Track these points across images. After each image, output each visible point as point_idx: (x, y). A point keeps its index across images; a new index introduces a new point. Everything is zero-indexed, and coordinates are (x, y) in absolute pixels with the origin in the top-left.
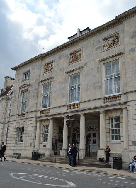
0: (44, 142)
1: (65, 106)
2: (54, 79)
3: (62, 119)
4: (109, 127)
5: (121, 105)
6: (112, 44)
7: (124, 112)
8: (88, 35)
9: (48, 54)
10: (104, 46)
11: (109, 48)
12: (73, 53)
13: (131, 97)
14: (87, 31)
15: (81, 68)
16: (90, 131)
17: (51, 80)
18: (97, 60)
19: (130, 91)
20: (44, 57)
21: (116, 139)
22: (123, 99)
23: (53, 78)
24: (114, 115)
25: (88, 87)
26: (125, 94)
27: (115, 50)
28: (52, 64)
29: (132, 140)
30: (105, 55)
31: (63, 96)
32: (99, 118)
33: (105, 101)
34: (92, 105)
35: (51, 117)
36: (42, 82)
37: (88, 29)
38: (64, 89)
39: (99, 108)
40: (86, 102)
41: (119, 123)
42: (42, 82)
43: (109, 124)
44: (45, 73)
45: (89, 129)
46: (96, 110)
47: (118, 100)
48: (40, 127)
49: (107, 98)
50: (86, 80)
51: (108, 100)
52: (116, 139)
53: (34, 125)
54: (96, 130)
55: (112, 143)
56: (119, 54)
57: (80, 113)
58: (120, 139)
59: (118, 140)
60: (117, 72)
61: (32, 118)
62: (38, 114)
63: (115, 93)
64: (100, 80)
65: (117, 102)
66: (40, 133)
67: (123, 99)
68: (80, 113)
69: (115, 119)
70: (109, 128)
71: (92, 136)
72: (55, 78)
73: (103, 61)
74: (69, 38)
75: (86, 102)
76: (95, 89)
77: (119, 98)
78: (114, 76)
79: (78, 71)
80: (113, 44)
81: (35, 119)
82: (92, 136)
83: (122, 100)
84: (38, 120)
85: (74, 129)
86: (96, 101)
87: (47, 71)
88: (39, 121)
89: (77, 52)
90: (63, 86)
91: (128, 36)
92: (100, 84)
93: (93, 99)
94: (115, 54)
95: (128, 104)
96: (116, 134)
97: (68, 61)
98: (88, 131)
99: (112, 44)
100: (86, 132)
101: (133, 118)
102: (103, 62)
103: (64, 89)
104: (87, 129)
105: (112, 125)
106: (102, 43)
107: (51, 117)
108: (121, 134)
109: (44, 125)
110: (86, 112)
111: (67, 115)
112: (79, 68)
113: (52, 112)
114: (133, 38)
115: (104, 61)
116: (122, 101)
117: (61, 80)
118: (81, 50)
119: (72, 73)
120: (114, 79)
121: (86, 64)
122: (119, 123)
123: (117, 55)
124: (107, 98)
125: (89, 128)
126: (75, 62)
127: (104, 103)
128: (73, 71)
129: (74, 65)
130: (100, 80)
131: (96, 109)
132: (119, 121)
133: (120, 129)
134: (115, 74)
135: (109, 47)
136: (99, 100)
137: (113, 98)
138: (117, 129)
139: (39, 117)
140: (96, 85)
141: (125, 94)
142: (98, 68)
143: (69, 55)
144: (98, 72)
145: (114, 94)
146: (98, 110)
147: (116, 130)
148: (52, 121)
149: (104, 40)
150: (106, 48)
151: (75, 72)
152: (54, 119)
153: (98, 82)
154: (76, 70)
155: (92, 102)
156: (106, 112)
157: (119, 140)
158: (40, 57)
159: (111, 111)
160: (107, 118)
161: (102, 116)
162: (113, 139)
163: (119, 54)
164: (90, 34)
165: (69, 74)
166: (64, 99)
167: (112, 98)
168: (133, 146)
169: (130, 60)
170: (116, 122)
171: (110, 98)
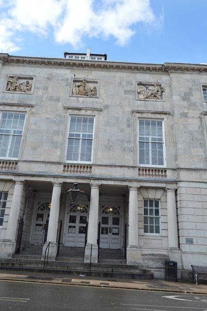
1: (60, 163)
2: (33, 110)
7: (170, 195)
8: (114, 66)
9: (24, 61)
10: (139, 93)
11: (146, 99)
12: (81, 81)
14: (103, 59)
15: (98, 111)
16: (42, 209)
17: (27, 109)
18: (128, 109)
19: (182, 167)
20: (12, 61)
21: (150, 232)
22: (170, 175)
23: (32, 106)
24: (152, 195)
25: (111, 144)
26: (173, 169)
27: (158, 105)
28: (30, 81)
29: (185, 235)
30: (140, 105)
31: (55, 145)
35: (23, 179)
37: (105, 56)
38: (57, 133)
39: (131, 181)
40: (106, 166)
41: (5, 201)
44: (8, 92)
45: (116, 211)
47: (12, 168)
51: (153, 172)
52: (152, 231)
54: (119, 214)
55: (147, 238)
57: (92, 182)
59: (154, 234)
60: (159, 136)
64: (132, 139)
67: (170, 175)
68: (92, 182)
69: (151, 201)
71: (78, 220)
72: (35, 108)
73: (138, 112)
74: (66, 54)
75: (106, 166)
76: (124, 150)
78: (12, 132)
79: (89, 113)
80: (154, 96)
85: (104, 208)
86: (126, 169)
87: (15, 90)
89: (88, 82)
90: (56, 128)
91: (178, 95)
92: (132, 145)
93: (119, 165)
94: (153, 110)
95: (180, 184)
96: (151, 223)
98: (70, 211)
100: (100, 215)
103: (57, 133)
104: (102, 211)
106: (134, 87)
107: (23, 179)
110: (104, 182)
111: (62, 180)
112: (94, 109)
113: (22, 168)
115: (139, 114)
117: (52, 116)
119: (76, 112)
121: (107, 107)
122: (5, 201)
124: (144, 169)
125: (42, 205)
128: (80, 109)
129: (81, 99)
130: (132, 139)
131: (125, 182)
132: (6, 198)
133: (4, 210)
134: (17, 130)
135: (147, 98)
136: (131, 169)
137: (11, 164)
141: (173, 169)
142: (128, 121)
144: (129, 126)
146: (129, 184)
148: (136, 192)
150: (141, 97)
151: (83, 112)
152: (27, 185)
153: (130, 142)
154: (86, 109)
155: (118, 169)
156: (140, 189)
157: (157, 234)
158: (4, 57)
159: (147, 188)
160: (141, 198)
161: (133, 196)
162: (146, 231)
163: (165, 114)
164: (131, 67)
165: (70, 111)
166: (58, 152)
168: (188, 245)
169: (181, 127)
170: (151, 207)
171: (10, 163)
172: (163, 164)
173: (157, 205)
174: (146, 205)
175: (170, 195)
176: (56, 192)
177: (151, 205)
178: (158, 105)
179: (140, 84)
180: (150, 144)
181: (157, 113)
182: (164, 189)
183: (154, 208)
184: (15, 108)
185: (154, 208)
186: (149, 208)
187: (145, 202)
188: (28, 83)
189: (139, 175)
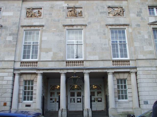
0: (25, 101)
1: (63, 61)
2: (44, 28)
3: (58, 76)
4: (128, 86)
5: (61, 70)
6: (118, 14)
7: (133, 76)
12: (72, 8)
13: (140, 63)
17: (40, 28)
18: (104, 23)
21: (122, 99)
23: (43, 26)
24: (122, 76)
27: (35, 22)
30: (111, 20)
32: (59, 78)
33: (22, 64)
34: (101, 65)
35: (42, 72)
36: (23, 26)
39: (61, 69)
42: (23, 26)
43: (23, 86)
46: (105, 71)
47: (25, 65)
48: (20, 82)
49: (32, 62)
50: (90, 39)
52: (123, 99)
53: (11, 78)
56: (126, 25)
57: (84, 71)
58: (126, 98)
59: (124, 100)
61: (6, 70)
62: (18, 66)
63: (32, 58)
65: (126, 66)
66: (19, 90)
67: (132, 64)
68: (84, 71)
70: (23, 90)
71: (76, 95)
77: (36, 64)
79: (79, 27)
80: (119, 14)
81: (12, 70)
82: (76, 95)
83: (131, 64)
84: (16, 72)
87: (31, 16)
88: (19, 74)
96: (122, 94)
97: (65, 14)
99: (118, 14)
101: (143, 82)
102: (110, 27)
105: (118, 86)
106: (106, 10)
108: (34, 96)
109: (24, 80)
114: (138, 16)
116: (131, 66)
118: (41, 9)
119: (71, 28)
120: (32, 46)
121: (89, 23)
123: (81, 25)
124: (70, 61)
126: (76, 17)
127: (21, 66)
128: (73, 26)
132: (32, 84)
138: (29, 91)
139: (19, 70)
140: (104, 46)
143: (65, 8)
145: (30, 60)
146: (108, 71)
147: (29, 92)
149: (108, 8)
151: (75, 27)
152: (44, 75)
154: (77, 25)
161: (110, 78)
162: (119, 98)
163: (126, 25)
167: (29, 63)
170: (122, 84)
172: (127, 57)
173: (125, 83)
174: (118, 83)
175: (133, 76)
176: (63, 79)
177: (121, 83)
178: (121, 20)
179: (109, 7)
180: (118, 45)
181: (118, 25)
182: (129, 72)
183: (123, 84)
184: (32, 28)
185: (27, 86)
186: (120, 84)
187: (118, 80)
188: (39, 11)
189: (113, 65)
